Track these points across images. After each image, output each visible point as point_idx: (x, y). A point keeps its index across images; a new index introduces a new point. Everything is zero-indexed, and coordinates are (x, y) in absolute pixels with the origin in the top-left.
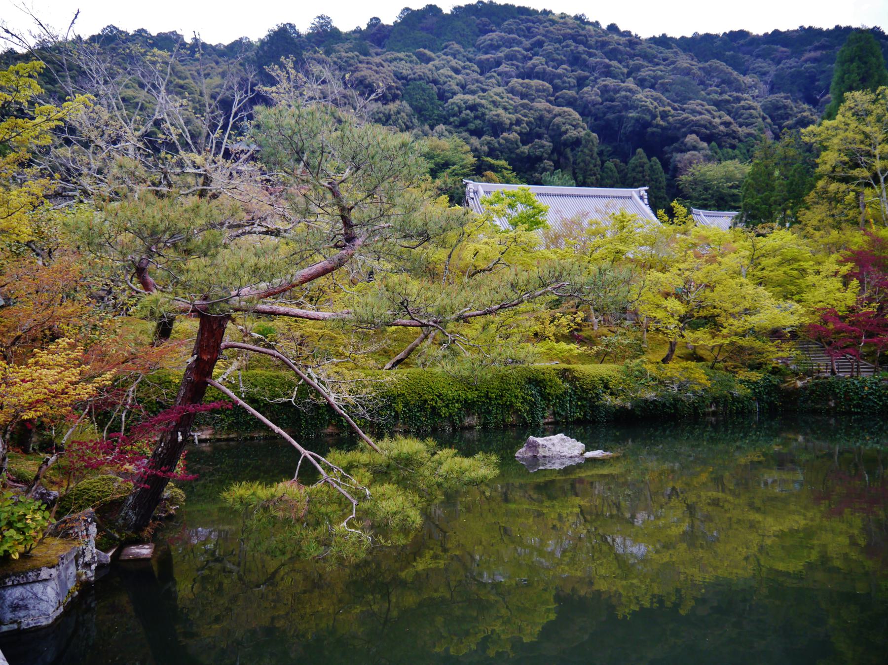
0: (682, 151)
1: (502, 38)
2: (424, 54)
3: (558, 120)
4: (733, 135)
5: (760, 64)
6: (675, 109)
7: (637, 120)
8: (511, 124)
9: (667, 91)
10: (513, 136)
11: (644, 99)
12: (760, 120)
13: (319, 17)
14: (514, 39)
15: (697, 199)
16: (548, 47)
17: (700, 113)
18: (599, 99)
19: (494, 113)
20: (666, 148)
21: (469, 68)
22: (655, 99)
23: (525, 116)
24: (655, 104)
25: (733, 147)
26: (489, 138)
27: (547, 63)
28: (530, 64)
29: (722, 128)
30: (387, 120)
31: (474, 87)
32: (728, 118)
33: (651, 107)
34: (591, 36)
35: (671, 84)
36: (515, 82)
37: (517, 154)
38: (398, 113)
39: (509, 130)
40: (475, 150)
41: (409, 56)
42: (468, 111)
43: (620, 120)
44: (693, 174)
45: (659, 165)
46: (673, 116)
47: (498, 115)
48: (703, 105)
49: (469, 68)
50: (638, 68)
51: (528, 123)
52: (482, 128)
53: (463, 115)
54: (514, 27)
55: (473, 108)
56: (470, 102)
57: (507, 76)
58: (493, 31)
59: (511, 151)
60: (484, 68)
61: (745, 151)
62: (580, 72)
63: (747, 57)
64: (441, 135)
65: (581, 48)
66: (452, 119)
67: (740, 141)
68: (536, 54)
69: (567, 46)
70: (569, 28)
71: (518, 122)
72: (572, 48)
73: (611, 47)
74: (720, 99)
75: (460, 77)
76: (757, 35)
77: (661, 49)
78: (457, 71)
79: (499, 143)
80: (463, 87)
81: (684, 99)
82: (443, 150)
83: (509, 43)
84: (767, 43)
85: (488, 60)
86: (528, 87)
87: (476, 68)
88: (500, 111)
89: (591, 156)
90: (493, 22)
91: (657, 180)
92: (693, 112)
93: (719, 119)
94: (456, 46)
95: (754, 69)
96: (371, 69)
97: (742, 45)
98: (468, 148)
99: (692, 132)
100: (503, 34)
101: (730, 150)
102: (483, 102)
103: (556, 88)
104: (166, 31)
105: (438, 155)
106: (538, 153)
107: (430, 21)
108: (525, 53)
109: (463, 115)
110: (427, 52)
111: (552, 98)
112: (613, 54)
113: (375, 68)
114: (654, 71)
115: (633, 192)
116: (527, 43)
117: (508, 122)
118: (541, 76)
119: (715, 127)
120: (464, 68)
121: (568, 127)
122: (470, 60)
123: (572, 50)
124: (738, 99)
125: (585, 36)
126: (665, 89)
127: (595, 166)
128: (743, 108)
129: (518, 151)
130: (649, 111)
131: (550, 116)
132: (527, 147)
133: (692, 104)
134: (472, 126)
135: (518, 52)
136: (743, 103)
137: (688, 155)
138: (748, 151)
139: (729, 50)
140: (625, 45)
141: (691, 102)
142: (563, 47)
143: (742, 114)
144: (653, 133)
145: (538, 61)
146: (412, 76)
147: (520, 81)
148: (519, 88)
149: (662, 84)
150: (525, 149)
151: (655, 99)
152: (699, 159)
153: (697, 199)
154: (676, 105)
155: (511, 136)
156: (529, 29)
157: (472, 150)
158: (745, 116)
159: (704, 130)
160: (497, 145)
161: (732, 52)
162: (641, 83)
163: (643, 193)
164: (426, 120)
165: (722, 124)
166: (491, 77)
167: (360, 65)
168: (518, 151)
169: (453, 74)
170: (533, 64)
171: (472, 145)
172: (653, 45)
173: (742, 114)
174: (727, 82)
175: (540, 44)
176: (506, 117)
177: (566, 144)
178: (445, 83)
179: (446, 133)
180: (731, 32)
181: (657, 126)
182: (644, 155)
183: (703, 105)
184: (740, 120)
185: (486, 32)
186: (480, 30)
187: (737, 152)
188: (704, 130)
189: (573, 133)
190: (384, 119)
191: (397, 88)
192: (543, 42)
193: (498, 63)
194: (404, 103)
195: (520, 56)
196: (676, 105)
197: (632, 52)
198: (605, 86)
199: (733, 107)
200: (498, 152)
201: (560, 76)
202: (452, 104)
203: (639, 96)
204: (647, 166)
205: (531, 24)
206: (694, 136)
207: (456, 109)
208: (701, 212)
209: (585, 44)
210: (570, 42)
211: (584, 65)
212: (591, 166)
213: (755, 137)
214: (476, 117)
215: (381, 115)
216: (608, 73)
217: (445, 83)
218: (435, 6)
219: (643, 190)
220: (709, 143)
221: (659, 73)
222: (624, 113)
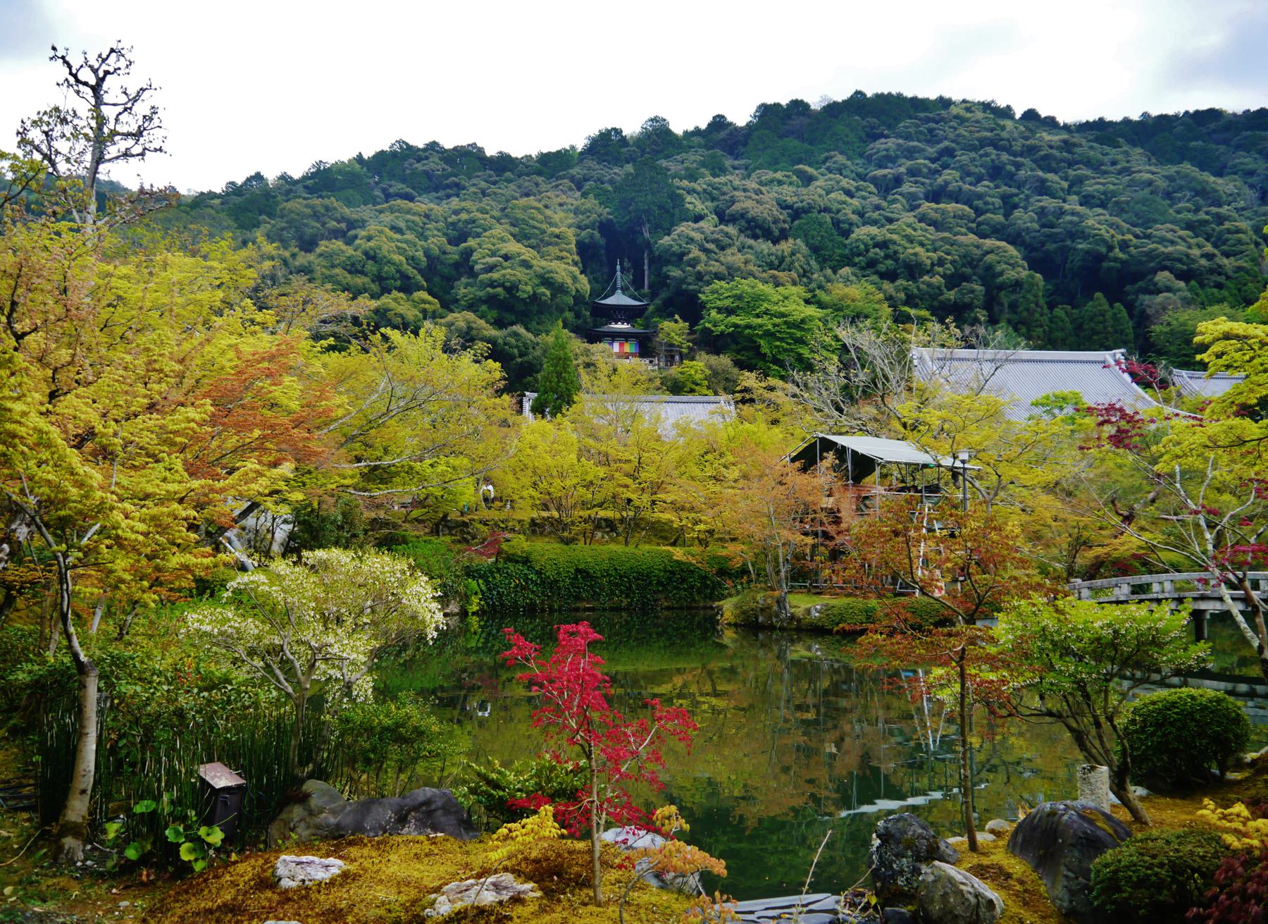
0: (1151, 293)
1: (899, 146)
2: (805, 172)
3: (990, 258)
4: (1218, 270)
5: (1242, 160)
6: (1137, 236)
7: (1087, 252)
8: (933, 265)
9: (1122, 211)
10: (937, 280)
11: (1097, 226)
12: (1252, 246)
13: (652, 120)
14: (914, 147)
15: (1175, 355)
16: (963, 157)
17: (1173, 243)
18: (1036, 226)
19: (911, 251)
20: (1128, 288)
21: (864, 189)
22: (1111, 225)
23: (948, 254)
24: (1112, 232)
25: (1219, 286)
26: (905, 283)
27: (962, 178)
28: (940, 180)
29: (1203, 262)
30: (780, 264)
31: (875, 215)
32: (1209, 248)
33: (1107, 236)
34: (1014, 140)
35: (1128, 203)
36: (927, 207)
37: (941, 302)
38: (793, 254)
39: (930, 272)
40: (889, 298)
41: (788, 177)
42: (877, 250)
43: (1065, 251)
44: (1169, 324)
45: (1124, 313)
46: (1136, 247)
47: (915, 254)
48: (1175, 232)
49: (864, 189)
50: (1080, 180)
51: (953, 262)
52: (895, 270)
53: (871, 254)
54: (912, 130)
55: (883, 245)
56: (879, 238)
57: (911, 197)
58: (887, 137)
59: (933, 297)
60: (887, 187)
61: (1235, 292)
62: (1006, 188)
63: (1222, 148)
64: (847, 281)
65: (1005, 157)
66: (857, 260)
67: (1228, 277)
68: (945, 166)
69: (987, 155)
70: (986, 129)
71: (941, 262)
72: (993, 157)
73: (1042, 153)
74: (1195, 218)
75: (855, 202)
76: (1234, 115)
77: (1107, 149)
78: (849, 193)
79: (918, 288)
80: (861, 214)
81: (1147, 223)
82: (853, 301)
83: (910, 154)
84: (1252, 128)
85: (885, 176)
86: (944, 212)
87: (872, 188)
88: (919, 249)
89: (1037, 304)
90: (883, 123)
91: (1122, 332)
92: (1162, 240)
93: (1197, 250)
94: (840, 159)
95: (1235, 166)
96: (750, 198)
97: (1214, 131)
98: (881, 296)
99: (1164, 268)
100: (901, 141)
101: (1215, 290)
102: (895, 237)
103: (979, 212)
104: (464, 143)
105: (848, 306)
106: (967, 299)
107: (796, 122)
108: (933, 166)
109: (871, 254)
110: (807, 168)
111: (974, 225)
112: (1046, 163)
113: (755, 197)
114: (1104, 184)
115: (1107, 356)
116: (931, 151)
117: (929, 262)
118: (956, 197)
119: (1194, 261)
120: (858, 189)
121: (1005, 266)
122: (862, 177)
123: (993, 161)
124: (1220, 219)
125: (1008, 140)
126: (1120, 210)
127: (1042, 315)
128: (1229, 231)
129: (941, 298)
130: (1104, 241)
131: (979, 252)
132: (952, 292)
133: (1160, 230)
134: (881, 268)
135: (925, 165)
136: (1227, 225)
137: (1160, 298)
138: (1239, 290)
139: (1196, 139)
140: (1060, 149)
141: (1158, 226)
142: (981, 156)
143: (1227, 240)
144: (1109, 269)
145: (949, 175)
146: (800, 205)
147: (934, 205)
148: (933, 215)
149: (1117, 203)
150: (951, 295)
151: (1111, 225)
152: (1175, 303)
153: (1175, 355)
154: (1138, 230)
155: (934, 280)
156: (931, 131)
157: (887, 299)
158: (1230, 242)
159: (1179, 265)
160: (915, 291)
161: (1200, 143)
162: (1086, 201)
163: (1118, 356)
164: (825, 260)
165: (1203, 256)
166: (895, 201)
167: (736, 193)
168: (941, 298)
169: (848, 199)
170: (945, 181)
171: (885, 292)
172: (1095, 145)
173: (1227, 240)
174: (1203, 193)
175: (950, 152)
176: (925, 256)
177: (1001, 287)
178: (839, 211)
179: (853, 278)
180: (1197, 112)
181: (1116, 259)
182: (1104, 300)
183: (1175, 232)
184: (1225, 248)
185: (876, 137)
186: (868, 135)
187: (1225, 293)
188: (1179, 265)
189: (1011, 274)
190: (776, 262)
191: (784, 222)
192: (954, 150)
193: (898, 181)
194: (798, 241)
195: (925, 170)
196: (1138, 230)
197: (1069, 156)
198: (1043, 208)
199: (1213, 230)
200: (917, 300)
201: (980, 196)
202: (857, 241)
203: (1090, 222)
204: (1109, 315)
205: (932, 125)
206: (1167, 274)
207: (862, 247)
208: (1184, 373)
209: (1008, 150)
210: (990, 149)
211: (1010, 179)
212: (1037, 315)
213: (1247, 271)
214: (887, 257)
215: (773, 258)
216: (1043, 189)
217: (839, 211)
218: (802, 101)
219: (1119, 353)
220: (1187, 282)
221: (1111, 187)
222: (1069, 243)
